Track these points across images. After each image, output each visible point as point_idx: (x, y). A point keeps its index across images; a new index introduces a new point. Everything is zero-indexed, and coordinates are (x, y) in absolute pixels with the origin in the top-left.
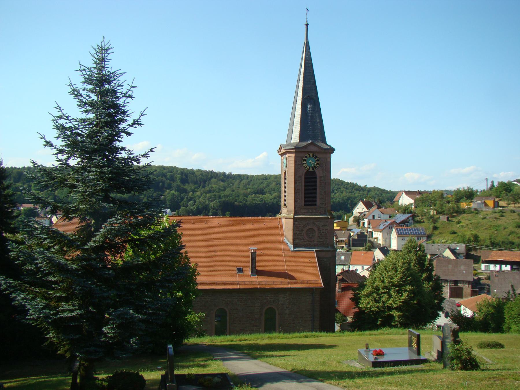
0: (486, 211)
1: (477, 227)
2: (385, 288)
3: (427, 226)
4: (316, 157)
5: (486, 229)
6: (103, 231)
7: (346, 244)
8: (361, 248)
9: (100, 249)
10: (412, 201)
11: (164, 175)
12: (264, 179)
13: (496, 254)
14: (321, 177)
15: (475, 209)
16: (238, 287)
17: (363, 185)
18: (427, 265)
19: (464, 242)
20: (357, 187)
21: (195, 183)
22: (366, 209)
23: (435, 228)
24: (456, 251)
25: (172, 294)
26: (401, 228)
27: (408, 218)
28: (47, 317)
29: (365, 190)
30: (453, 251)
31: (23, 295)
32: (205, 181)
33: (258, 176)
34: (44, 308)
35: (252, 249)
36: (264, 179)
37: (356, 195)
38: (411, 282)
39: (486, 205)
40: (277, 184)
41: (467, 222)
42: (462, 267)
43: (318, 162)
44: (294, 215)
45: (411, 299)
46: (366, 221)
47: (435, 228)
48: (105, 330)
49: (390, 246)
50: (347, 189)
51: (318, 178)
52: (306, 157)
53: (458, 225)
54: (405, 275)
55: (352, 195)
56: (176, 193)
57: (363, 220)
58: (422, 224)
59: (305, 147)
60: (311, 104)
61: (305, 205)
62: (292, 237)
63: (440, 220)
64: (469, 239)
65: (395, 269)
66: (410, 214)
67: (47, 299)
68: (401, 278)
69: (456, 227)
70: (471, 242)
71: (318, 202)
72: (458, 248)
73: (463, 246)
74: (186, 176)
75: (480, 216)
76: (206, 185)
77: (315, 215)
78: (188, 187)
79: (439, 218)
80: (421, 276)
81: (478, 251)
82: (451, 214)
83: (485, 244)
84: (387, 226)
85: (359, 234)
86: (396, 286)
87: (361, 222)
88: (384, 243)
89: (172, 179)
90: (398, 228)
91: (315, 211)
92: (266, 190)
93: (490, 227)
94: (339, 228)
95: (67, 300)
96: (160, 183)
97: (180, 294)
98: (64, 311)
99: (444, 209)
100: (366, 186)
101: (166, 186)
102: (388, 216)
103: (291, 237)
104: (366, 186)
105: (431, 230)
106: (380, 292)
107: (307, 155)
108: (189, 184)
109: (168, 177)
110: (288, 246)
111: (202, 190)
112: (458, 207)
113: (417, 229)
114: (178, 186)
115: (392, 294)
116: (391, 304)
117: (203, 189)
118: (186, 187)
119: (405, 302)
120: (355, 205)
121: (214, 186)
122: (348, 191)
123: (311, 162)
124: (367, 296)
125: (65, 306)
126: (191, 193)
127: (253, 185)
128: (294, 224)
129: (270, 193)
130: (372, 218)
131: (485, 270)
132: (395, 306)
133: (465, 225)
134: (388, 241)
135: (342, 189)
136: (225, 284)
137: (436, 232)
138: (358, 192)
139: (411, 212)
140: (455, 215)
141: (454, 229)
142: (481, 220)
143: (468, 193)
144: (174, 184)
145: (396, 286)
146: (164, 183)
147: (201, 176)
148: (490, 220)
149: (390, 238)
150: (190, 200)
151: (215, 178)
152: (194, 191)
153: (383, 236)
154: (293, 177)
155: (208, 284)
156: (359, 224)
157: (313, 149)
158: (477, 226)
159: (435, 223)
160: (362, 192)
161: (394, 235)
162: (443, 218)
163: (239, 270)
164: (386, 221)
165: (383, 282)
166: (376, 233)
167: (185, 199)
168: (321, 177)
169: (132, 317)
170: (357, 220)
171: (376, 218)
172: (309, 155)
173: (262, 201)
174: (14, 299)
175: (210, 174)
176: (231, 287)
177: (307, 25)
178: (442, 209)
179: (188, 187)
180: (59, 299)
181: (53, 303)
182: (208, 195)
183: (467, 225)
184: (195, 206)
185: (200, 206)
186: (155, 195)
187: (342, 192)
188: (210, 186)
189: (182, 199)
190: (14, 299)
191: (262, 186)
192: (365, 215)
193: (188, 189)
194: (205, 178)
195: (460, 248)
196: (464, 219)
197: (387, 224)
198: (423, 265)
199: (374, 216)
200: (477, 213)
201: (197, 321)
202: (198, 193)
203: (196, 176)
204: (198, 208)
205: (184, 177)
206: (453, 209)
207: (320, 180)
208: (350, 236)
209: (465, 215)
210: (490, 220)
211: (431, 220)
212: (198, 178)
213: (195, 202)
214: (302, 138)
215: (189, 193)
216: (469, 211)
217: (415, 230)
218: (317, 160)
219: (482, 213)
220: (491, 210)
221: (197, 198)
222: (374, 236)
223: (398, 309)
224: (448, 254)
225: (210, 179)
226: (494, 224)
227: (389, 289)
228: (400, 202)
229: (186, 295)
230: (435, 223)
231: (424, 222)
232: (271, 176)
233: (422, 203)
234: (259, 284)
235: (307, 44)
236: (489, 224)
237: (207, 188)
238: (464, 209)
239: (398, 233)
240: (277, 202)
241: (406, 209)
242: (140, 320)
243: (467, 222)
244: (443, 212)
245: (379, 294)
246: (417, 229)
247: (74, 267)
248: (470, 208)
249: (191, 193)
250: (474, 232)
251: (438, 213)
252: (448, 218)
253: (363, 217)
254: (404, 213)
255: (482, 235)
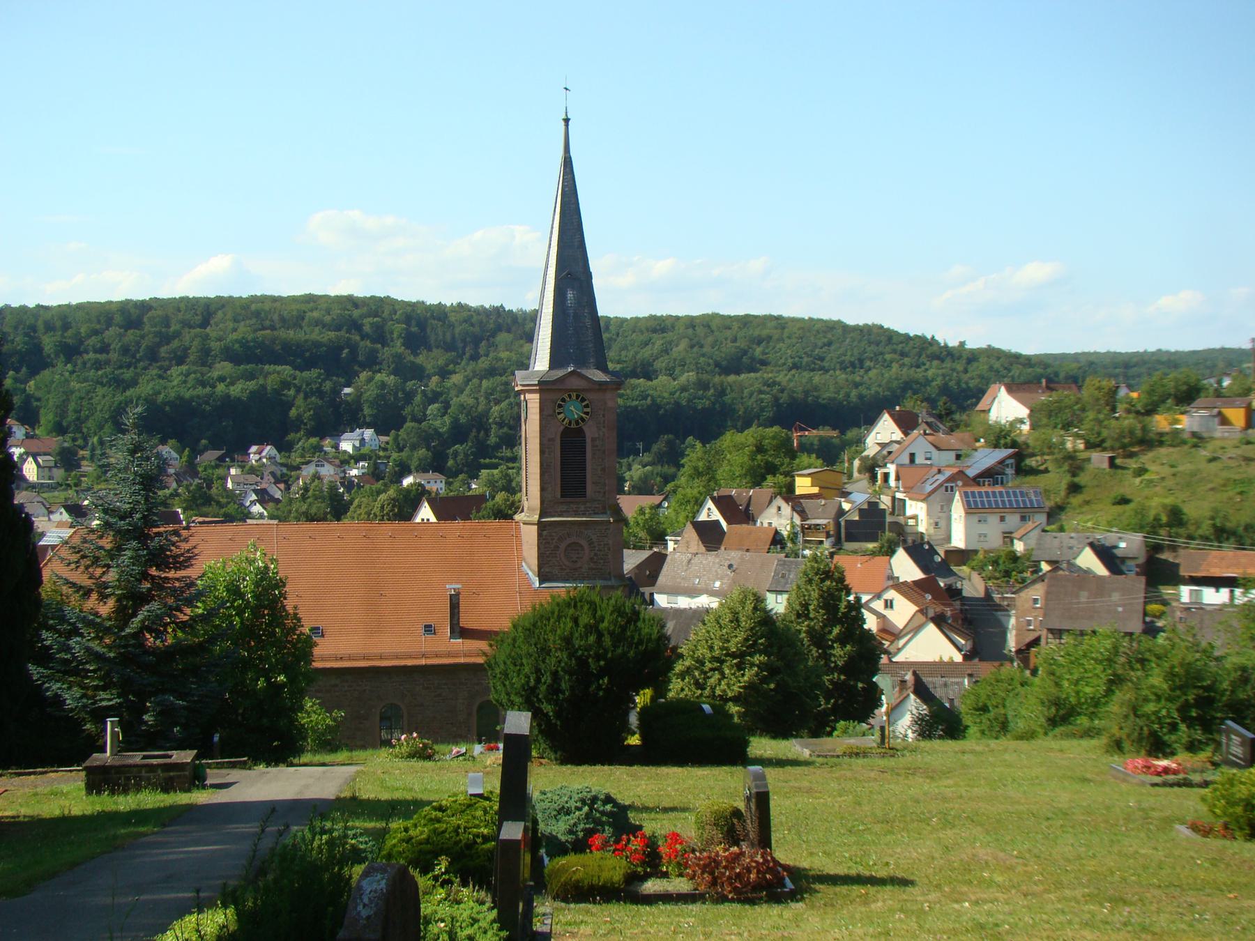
0: (1223, 439)
1: (1188, 485)
2: (714, 659)
3: (1057, 480)
4: (583, 400)
5: (1212, 489)
6: (140, 617)
7: (828, 536)
8: (871, 546)
9: (138, 635)
10: (1022, 411)
11: (355, 326)
12: (654, 331)
13: (1223, 561)
14: (593, 440)
15: (1194, 434)
16: (423, 662)
17: (953, 343)
18: (842, 610)
19: (1139, 528)
20: (935, 348)
21: (449, 347)
22: (898, 435)
23: (1074, 488)
24: (1115, 551)
25: (268, 680)
26: (976, 489)
27: (1002, 462)
28: (85, 706)
29: (960, 357)
30: (1105, 554)
31: (59, 685)
32: (477, 341)
33: (637, 319)
34: (81, 698)
35: (452, 587)
36: (654, 331)
37: (930, 373)
38: (766, 647)
39: (1224, 421)
40: (692, 347)
41: (1166, 471)
42: (1116, 597)
43: (588, 410)
44: (541, 516)
45: (764, 680)
46: (891, 469)
47: (1074, 488)
48: (146, 717)
49: (948, 539)
50: (903, 354)
51: (588, 440)
52: (563, 400)
53: (1138, 480)
54: (754, 634)
55: (919, 374)
56: (391, 380)
57: (885, 466)
58: (1040, 477)
59: (561, 380)
60: (573, 289)
61: (562, 496)
62: (536, 562)
63: (1090, 467)
64: (1157, 519)
65: (736, 620)
66: (1011, 451)
67: (82, 688)
68: (746, 640)
69: (1131, 485)
70: (1161, 526)
71: (590, 489)
72: (1123, 545)
73: (1138, 538)
74: (422, 325)
75: (1204, 453)
76: (481, 351)
77: (584, 515)
78: (429, 360)
79: (1089, 460)
80: (830, 632)
81: (1181, 552)
82: (1124, 447)
83: (1200, 532)
84: (941, 485)
85: (865, 506)
86: (733, 656)
87: (880, 472)
88: (932, 531)
89: (381, 336)
90: (969, 490)
91: (582, 508)
92: (659, 365)
93: (1224, 485)
94: (816, 490)
95: (104, 688)
96: (341, 349)
97: (282, 678)
98: (102, 700)
99: (1105, 433)
100: (962, 344)
101: (360, 358)
102: (952, 455)
103: (534, 562)
104: (962, 344)
105: (1063, 493)
106: (706, 669)
107: (566, 396)
108: (430, 349)
109: (367, 328)
110: (529, 579)
111: (469, 368)
112: (1144, 429)
113: (1021, 493)
114: (399, 357)
115: (727, 671)
116: (724, 691)
117: (472, 365)
118: (420, 360)
119: (750, 687)
120: (871, 421)
121: (504, 355)
122: (906, 360)
123: (574, 410)
124: (682, 676)
125: (102, 695)
126: (435, 379)
127: (622, 349)
128: (540, 535)
129: (671, 373)
130: (907, 461)
131: (1191, 603)
132: (730, 694)
133: (1156, 482)
134: (942, 524)
135: (888, 357)
136: (397, 657)
137: (1076, 500)
138: (935, 363)
139: (1014, 444)
140: (1135, 449)
141: (1126, 491)
142: (1203, 465)
143: (1184, 388)
144: (386, 353)
145: (733, 656)
146: (354, 349)
147: (465, 326)
148: (1232, 463)
149: (949, 518)
150: (433, 400)
151: (509, 331)
152: (444, 373)
153: (929, 514)
154: (538, 441)
155: (364, 658)
156: (873, 478)
157: (576, 383)
158: (1190, 481)
159: (1074, 475)
160: (948, 364)
161: (958, 509)
162: (1099, 459)
163: (429, 629)
164: (939, 471)
165: (711, 648)
166: (914, 503)
167: (418, 398)
168: (593, 440)
169: (172, 703)
170: (870, 468)
171: (918, 460)
172: (570, 396)
173: (645, 398)
174: (48, 689)
175: (493, 317)
176: (410, 663)
177: (567, 121)
178: (1099, 434)
179: (429, 360)
180: (96, 688)
181: (90, 693)
182: (485, 383)
183: (1163, 479)
184: (446, 418)
185: (463, 419)
186: (328, 385)
187: (889, 366)
188: (491, 355)
189: (409, 396)
190: (48, 689)
191: (646, 353)
192: (890, 453)
193: (429, 367)
194: (477, 329)
195: (1128, 543)
196: (1156, 462)
197: (941, 478)
198: (836, 608)
199: (912, 456)
200: (1195, 446)
201: (328, 726)
202: (456, 379)
203: (452, 326)
204: (455, 424)
205: (414, 329)
206: (1131, 432)
207: (593, 446)
208: (841, 512)
209: (1163, 451)
210: (1232, 463)
211: (1066, 467)
212: (457, 331)
213: (447, 405)
214: (555, 362)
215: (429, 377)
216: (1175, 439)
217: (1015, 496)
218: (587, 406)
219: (1210, 446)
220: (1239, 436)
221: (453, 393)
222: (909, 512)
223: (736, 700)
224: (1088, 560)
225: (493, 335)
226: (1237, 477)
227: (722, 662)
228: (993, 416)
229: (292, 680)
230: (1074, 475)
231: (1046, 471)
232: (677, 318)
233: (1050, 416)
234: (465, 656)
235: (568, 163)
236: (1225, 474)
237: (483, 363)
238: (1161, 434)
239: (968, 503)
240: (689, 401)
241: (1001, 436)
242: (184, 708)
243: (1166, 471)
244: (1103, 441)
245: (705, 673)
246: (1021, 493)
247: (112, 655)
248: (1177, 432)
249: (435, 379)
250: (1169, 501)
251: (1090, 446)
252: (1112, 459)
253: (884, 457)
254: (996, 446)
255: (1192, 510)
